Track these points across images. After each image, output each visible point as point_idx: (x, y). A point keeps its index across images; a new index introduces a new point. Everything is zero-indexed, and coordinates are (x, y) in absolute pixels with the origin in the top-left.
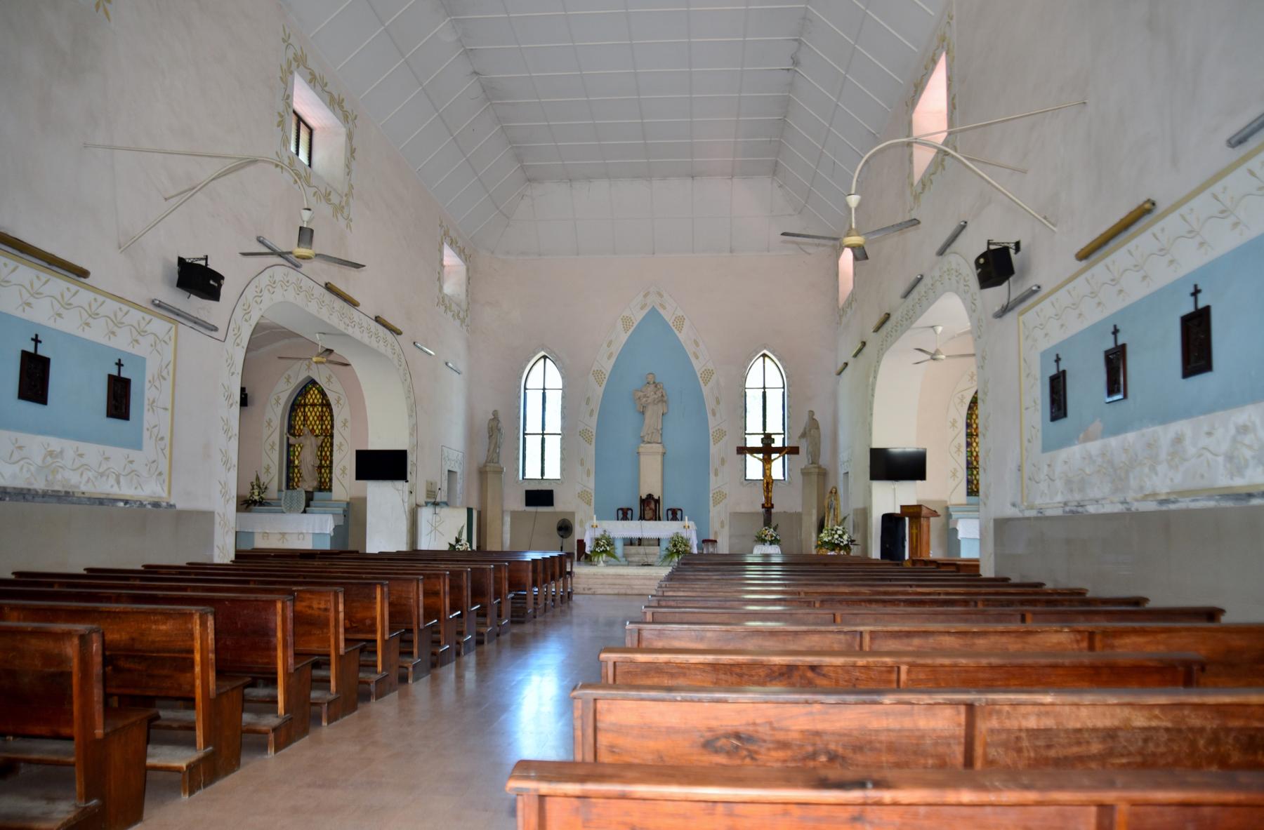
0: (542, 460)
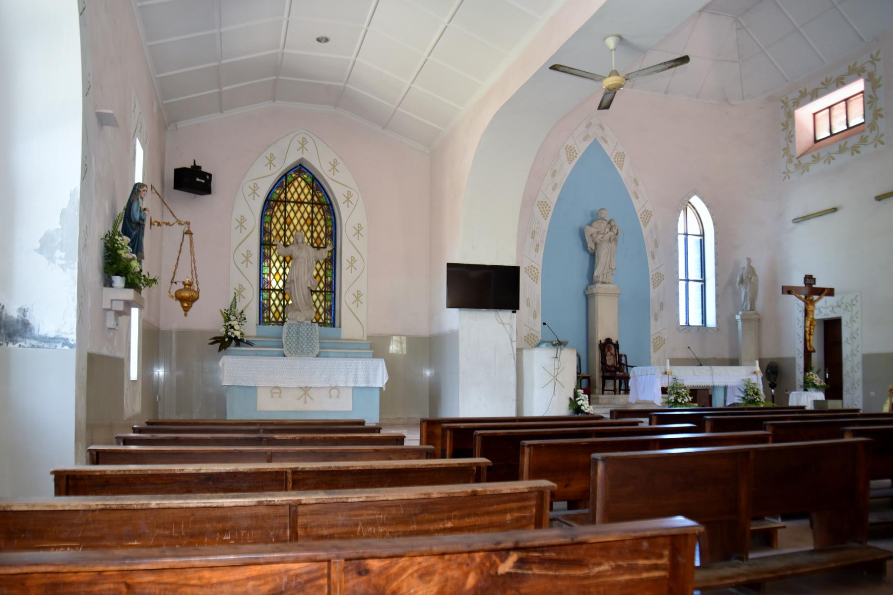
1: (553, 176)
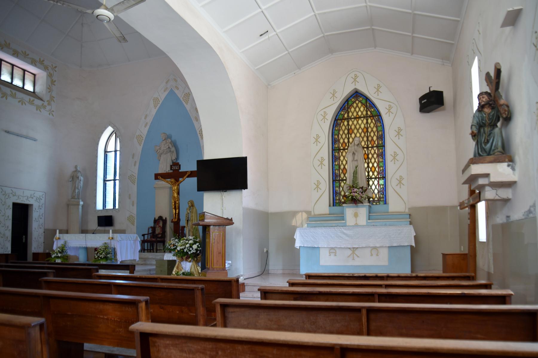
0: (106, 196)
1: (145, 118)
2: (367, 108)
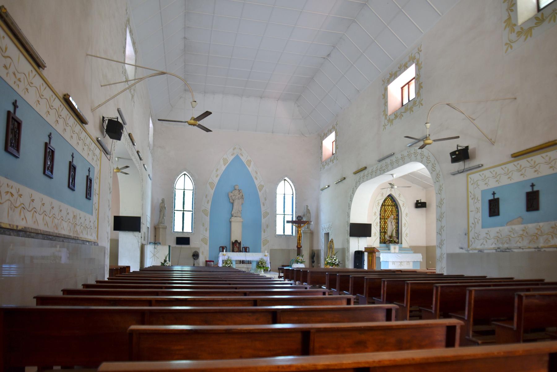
0: (183, 223)
1: (216, 171)
2: (392, 202)
